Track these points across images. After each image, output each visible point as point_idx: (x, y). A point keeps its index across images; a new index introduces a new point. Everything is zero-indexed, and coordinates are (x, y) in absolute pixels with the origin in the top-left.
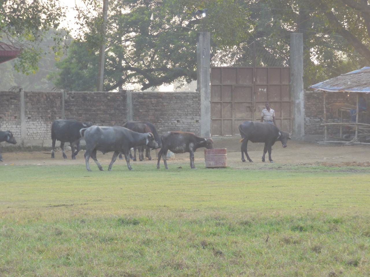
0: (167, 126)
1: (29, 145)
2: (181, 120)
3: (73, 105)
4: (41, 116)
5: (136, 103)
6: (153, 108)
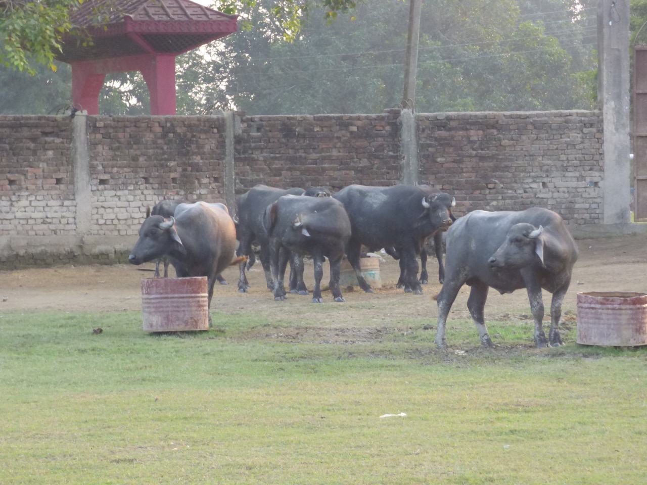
0: (511, 198)
1: (102, 248)
2: (551, 182)
3: (256, 148)
4: (143, 178)
5: (428, 142)
6: (474, 153)
